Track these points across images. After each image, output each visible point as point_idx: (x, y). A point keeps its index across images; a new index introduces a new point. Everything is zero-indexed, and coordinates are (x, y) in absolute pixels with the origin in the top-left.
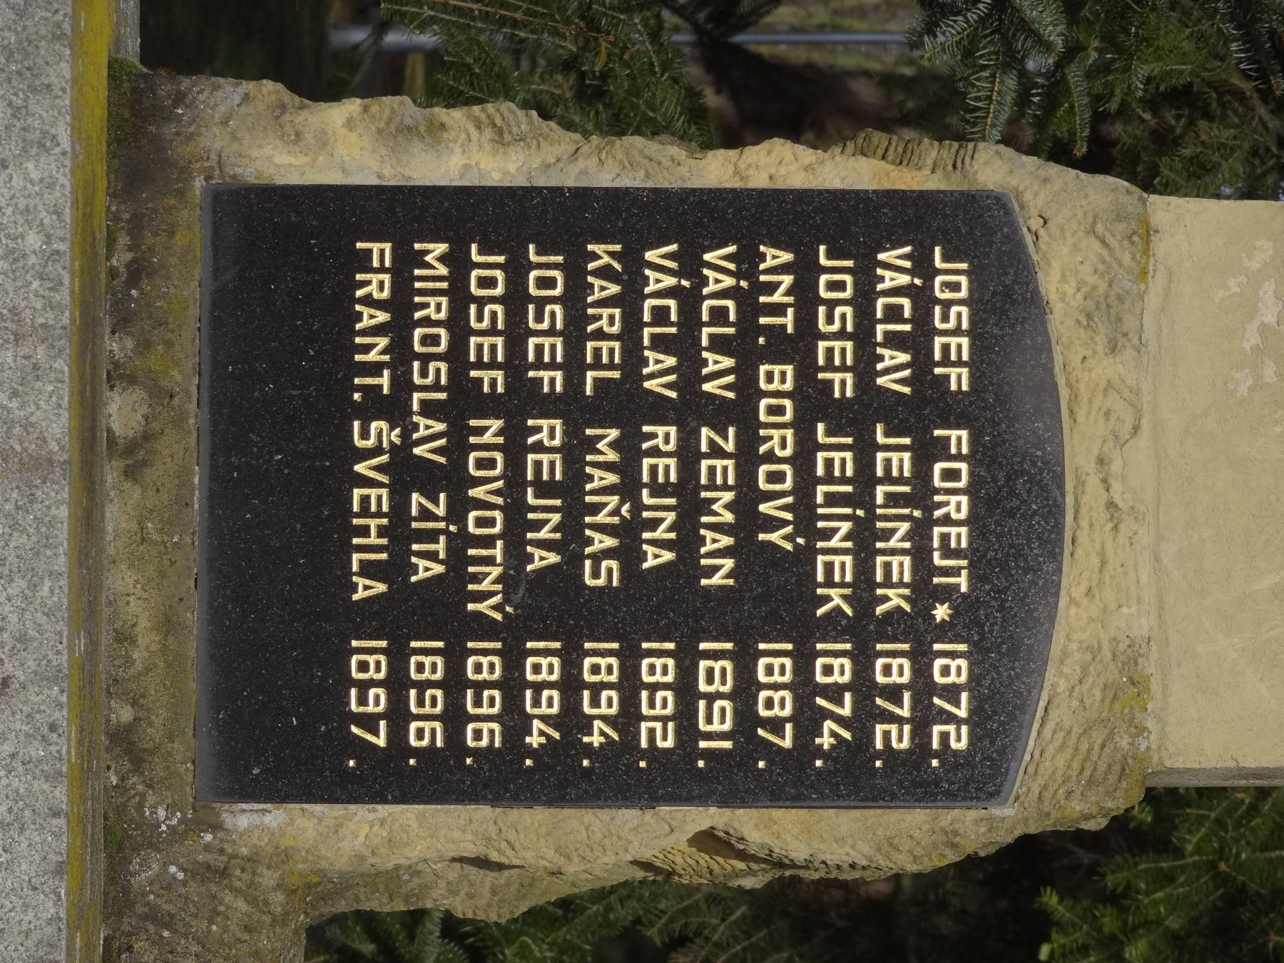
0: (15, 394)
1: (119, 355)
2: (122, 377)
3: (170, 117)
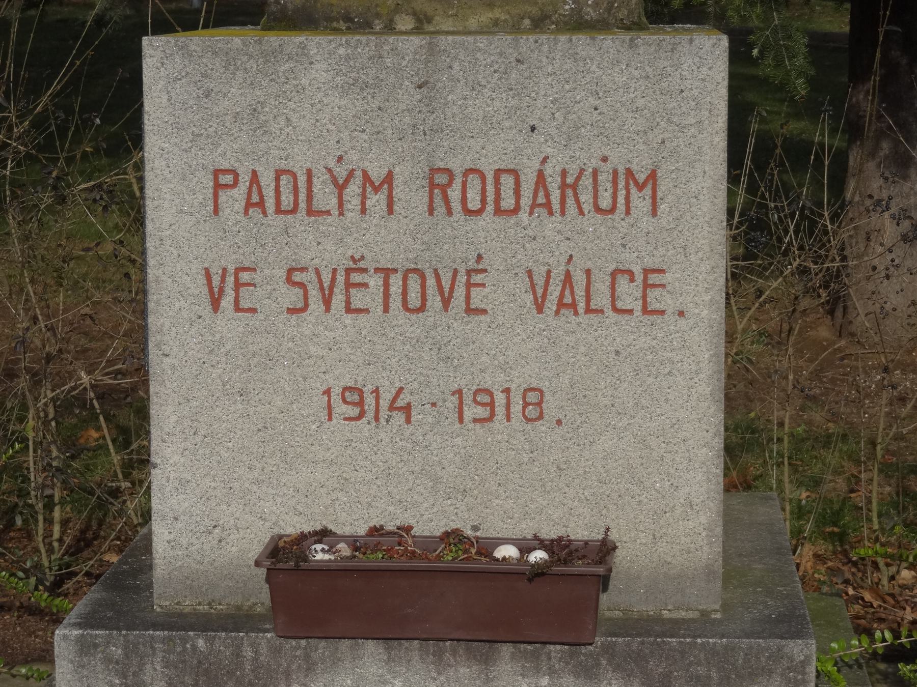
0: (403, 58)
1: (382, 26)
2: (390, 25)
3: (285, 5)
